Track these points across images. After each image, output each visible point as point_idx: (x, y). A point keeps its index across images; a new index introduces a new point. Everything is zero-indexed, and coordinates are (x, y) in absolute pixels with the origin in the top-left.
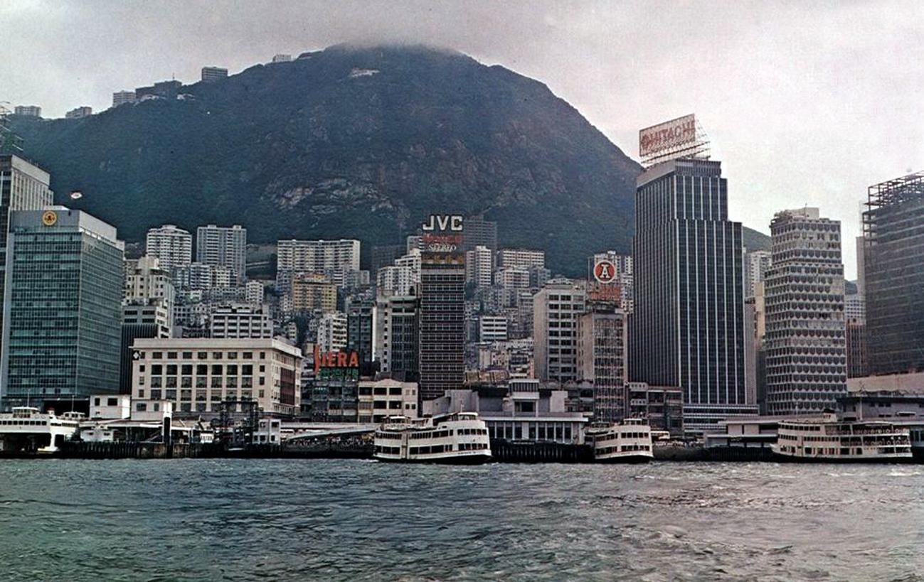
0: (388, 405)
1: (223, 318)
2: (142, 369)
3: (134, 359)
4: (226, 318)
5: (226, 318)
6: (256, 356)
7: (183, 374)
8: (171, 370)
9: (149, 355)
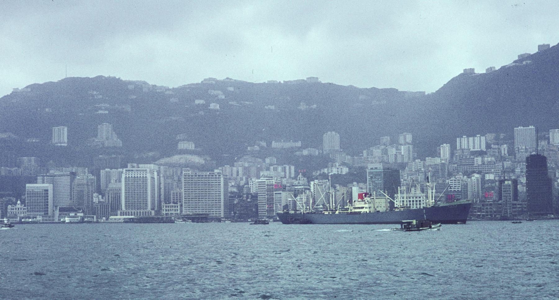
1: (452, 180)
6: (422, 198)
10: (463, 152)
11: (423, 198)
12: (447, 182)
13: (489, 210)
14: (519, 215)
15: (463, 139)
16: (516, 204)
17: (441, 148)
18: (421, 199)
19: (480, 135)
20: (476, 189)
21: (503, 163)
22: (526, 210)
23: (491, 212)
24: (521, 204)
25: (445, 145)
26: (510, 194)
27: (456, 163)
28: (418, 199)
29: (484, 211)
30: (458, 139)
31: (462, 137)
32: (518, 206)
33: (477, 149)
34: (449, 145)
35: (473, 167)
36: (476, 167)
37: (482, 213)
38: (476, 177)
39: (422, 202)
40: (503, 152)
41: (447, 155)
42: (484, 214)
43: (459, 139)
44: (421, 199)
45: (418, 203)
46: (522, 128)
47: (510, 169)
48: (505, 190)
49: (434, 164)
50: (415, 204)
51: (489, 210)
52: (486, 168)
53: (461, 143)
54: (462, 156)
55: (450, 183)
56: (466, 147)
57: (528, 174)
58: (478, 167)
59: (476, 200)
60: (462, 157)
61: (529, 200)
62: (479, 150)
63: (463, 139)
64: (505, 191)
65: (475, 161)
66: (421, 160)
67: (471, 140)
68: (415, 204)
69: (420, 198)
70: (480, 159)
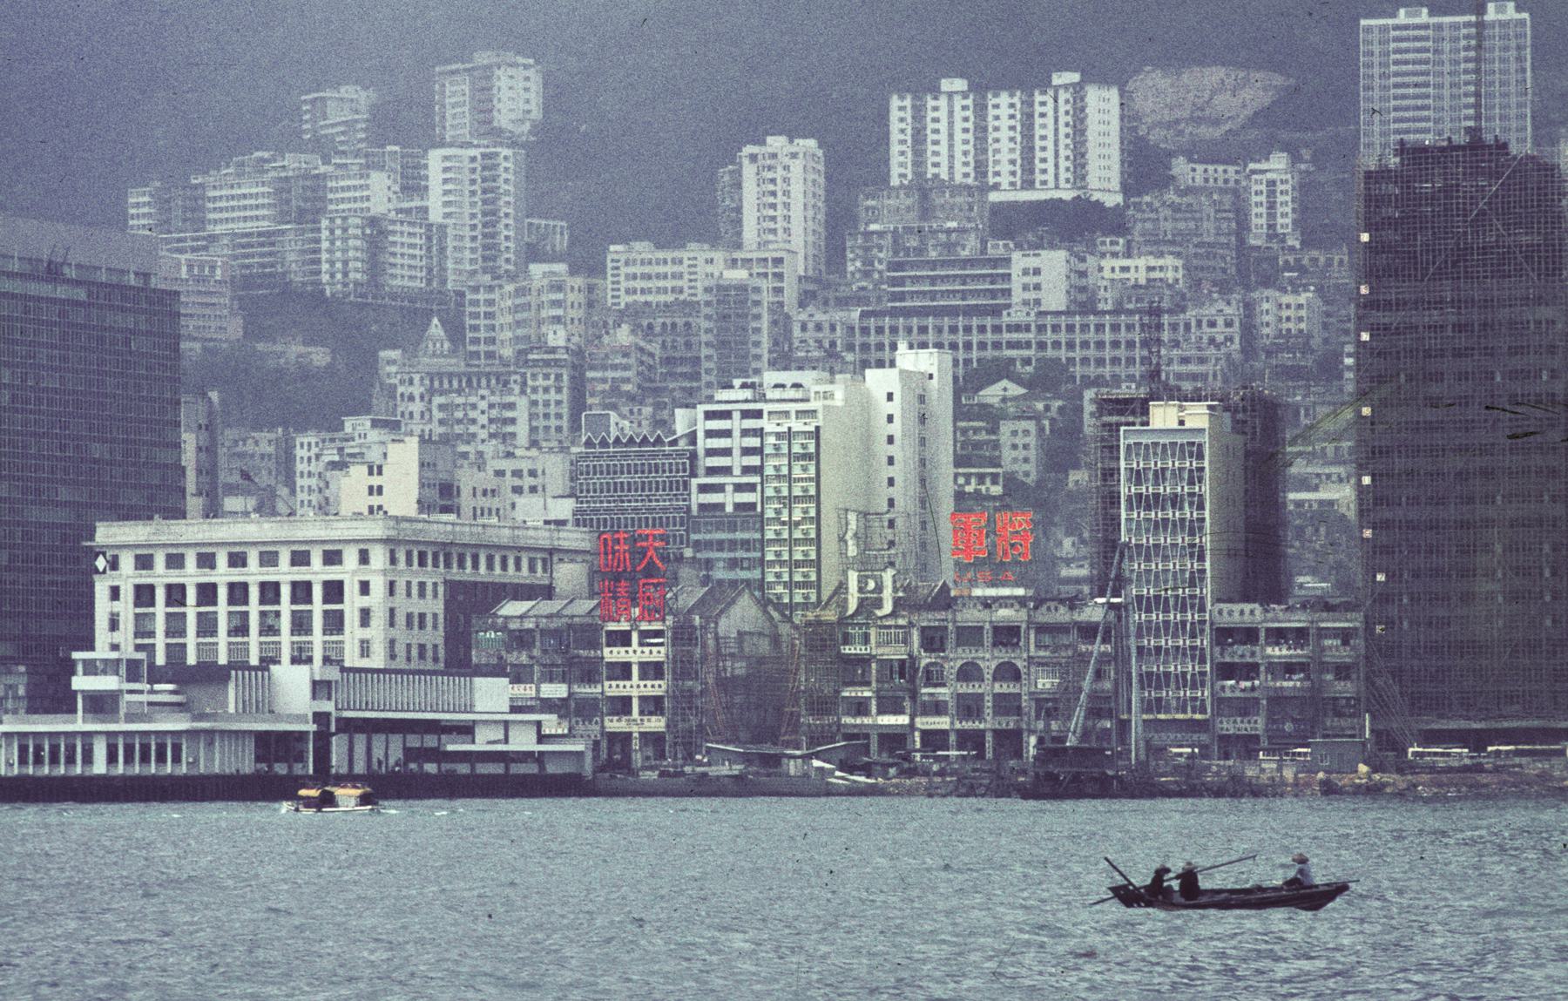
0: (635, 670)
1: (726, 415)
2: (115, 593)
3: (97, 571)
4: (736, 415)
5: (736, 415)
6: (351, 557)
7: (199, 604)
8: (299, 594)
9: (127, 562)
10: (926, 212)
11: (364, 558)
12: (681, 428)
13: (988, 688)
14: (1280, 745)
15: (937, 108)
16: (1249, 635)
17: (749, 170)
18: (348, 571)
19: (1075, 77)
20: (906, 496)
21: (1249, 307)
22: (1345, 688)
23: (1006, 705)
24: (1300, 635)
25: (776, 143)
26: (1195, 527)
27: (859, 299)
28: (317, 573)
29: (943, 693)
30: (895, 102)
31: (936, 91)
32: (1278, 652)
33: (1054, 187)
34: (812, 143)
35: (1042, 346)
36: (1017, 328)
37: (924, 723)
38: (906, 375)
39: (352, 603)
40: (1258, 221)
41: (797, 227)
42: (942, 723)
43: (908, 102)
44: (348, 571)
45: (318, 607)
46: (1424, 16)
47: (1306, 348)
48: (1147, 489)
49: (670, 298)
50: (285, 623)
51: (988, 688)
52: (1100, 345)
53: (919, 137)
54: (913, 242)
55: (703, 443)
56: (963, 172)
57: (1373, 330)
58: (1041, 329)
59: (862, 582)
60: (920, 251)
61: (1384, 597)
62: (1067, 195)
63: (943, 102)
64: (1155, 501)
65: (1016, 284)
66: (573, 272)
67: (1004, 112)
68: (285, 623)
69: (332, 558)
70: (1054, 263)
